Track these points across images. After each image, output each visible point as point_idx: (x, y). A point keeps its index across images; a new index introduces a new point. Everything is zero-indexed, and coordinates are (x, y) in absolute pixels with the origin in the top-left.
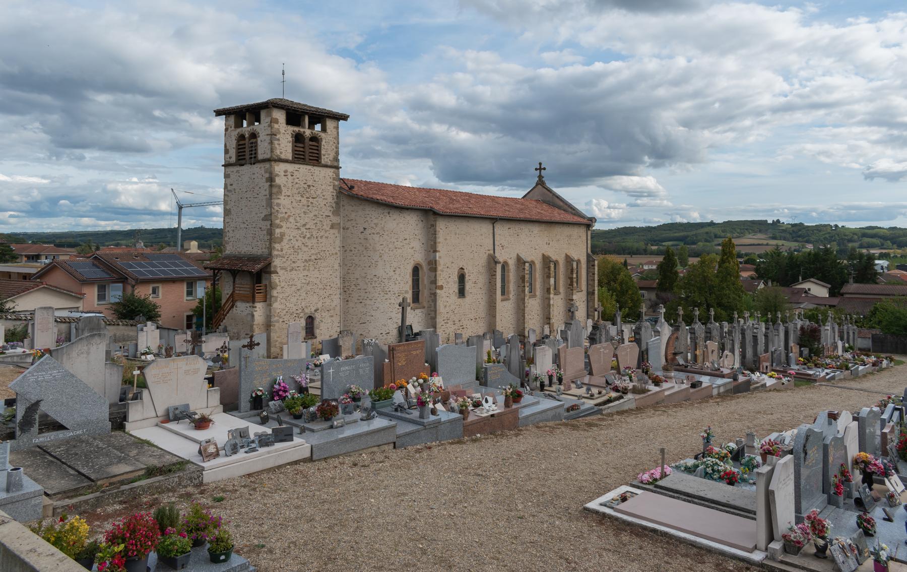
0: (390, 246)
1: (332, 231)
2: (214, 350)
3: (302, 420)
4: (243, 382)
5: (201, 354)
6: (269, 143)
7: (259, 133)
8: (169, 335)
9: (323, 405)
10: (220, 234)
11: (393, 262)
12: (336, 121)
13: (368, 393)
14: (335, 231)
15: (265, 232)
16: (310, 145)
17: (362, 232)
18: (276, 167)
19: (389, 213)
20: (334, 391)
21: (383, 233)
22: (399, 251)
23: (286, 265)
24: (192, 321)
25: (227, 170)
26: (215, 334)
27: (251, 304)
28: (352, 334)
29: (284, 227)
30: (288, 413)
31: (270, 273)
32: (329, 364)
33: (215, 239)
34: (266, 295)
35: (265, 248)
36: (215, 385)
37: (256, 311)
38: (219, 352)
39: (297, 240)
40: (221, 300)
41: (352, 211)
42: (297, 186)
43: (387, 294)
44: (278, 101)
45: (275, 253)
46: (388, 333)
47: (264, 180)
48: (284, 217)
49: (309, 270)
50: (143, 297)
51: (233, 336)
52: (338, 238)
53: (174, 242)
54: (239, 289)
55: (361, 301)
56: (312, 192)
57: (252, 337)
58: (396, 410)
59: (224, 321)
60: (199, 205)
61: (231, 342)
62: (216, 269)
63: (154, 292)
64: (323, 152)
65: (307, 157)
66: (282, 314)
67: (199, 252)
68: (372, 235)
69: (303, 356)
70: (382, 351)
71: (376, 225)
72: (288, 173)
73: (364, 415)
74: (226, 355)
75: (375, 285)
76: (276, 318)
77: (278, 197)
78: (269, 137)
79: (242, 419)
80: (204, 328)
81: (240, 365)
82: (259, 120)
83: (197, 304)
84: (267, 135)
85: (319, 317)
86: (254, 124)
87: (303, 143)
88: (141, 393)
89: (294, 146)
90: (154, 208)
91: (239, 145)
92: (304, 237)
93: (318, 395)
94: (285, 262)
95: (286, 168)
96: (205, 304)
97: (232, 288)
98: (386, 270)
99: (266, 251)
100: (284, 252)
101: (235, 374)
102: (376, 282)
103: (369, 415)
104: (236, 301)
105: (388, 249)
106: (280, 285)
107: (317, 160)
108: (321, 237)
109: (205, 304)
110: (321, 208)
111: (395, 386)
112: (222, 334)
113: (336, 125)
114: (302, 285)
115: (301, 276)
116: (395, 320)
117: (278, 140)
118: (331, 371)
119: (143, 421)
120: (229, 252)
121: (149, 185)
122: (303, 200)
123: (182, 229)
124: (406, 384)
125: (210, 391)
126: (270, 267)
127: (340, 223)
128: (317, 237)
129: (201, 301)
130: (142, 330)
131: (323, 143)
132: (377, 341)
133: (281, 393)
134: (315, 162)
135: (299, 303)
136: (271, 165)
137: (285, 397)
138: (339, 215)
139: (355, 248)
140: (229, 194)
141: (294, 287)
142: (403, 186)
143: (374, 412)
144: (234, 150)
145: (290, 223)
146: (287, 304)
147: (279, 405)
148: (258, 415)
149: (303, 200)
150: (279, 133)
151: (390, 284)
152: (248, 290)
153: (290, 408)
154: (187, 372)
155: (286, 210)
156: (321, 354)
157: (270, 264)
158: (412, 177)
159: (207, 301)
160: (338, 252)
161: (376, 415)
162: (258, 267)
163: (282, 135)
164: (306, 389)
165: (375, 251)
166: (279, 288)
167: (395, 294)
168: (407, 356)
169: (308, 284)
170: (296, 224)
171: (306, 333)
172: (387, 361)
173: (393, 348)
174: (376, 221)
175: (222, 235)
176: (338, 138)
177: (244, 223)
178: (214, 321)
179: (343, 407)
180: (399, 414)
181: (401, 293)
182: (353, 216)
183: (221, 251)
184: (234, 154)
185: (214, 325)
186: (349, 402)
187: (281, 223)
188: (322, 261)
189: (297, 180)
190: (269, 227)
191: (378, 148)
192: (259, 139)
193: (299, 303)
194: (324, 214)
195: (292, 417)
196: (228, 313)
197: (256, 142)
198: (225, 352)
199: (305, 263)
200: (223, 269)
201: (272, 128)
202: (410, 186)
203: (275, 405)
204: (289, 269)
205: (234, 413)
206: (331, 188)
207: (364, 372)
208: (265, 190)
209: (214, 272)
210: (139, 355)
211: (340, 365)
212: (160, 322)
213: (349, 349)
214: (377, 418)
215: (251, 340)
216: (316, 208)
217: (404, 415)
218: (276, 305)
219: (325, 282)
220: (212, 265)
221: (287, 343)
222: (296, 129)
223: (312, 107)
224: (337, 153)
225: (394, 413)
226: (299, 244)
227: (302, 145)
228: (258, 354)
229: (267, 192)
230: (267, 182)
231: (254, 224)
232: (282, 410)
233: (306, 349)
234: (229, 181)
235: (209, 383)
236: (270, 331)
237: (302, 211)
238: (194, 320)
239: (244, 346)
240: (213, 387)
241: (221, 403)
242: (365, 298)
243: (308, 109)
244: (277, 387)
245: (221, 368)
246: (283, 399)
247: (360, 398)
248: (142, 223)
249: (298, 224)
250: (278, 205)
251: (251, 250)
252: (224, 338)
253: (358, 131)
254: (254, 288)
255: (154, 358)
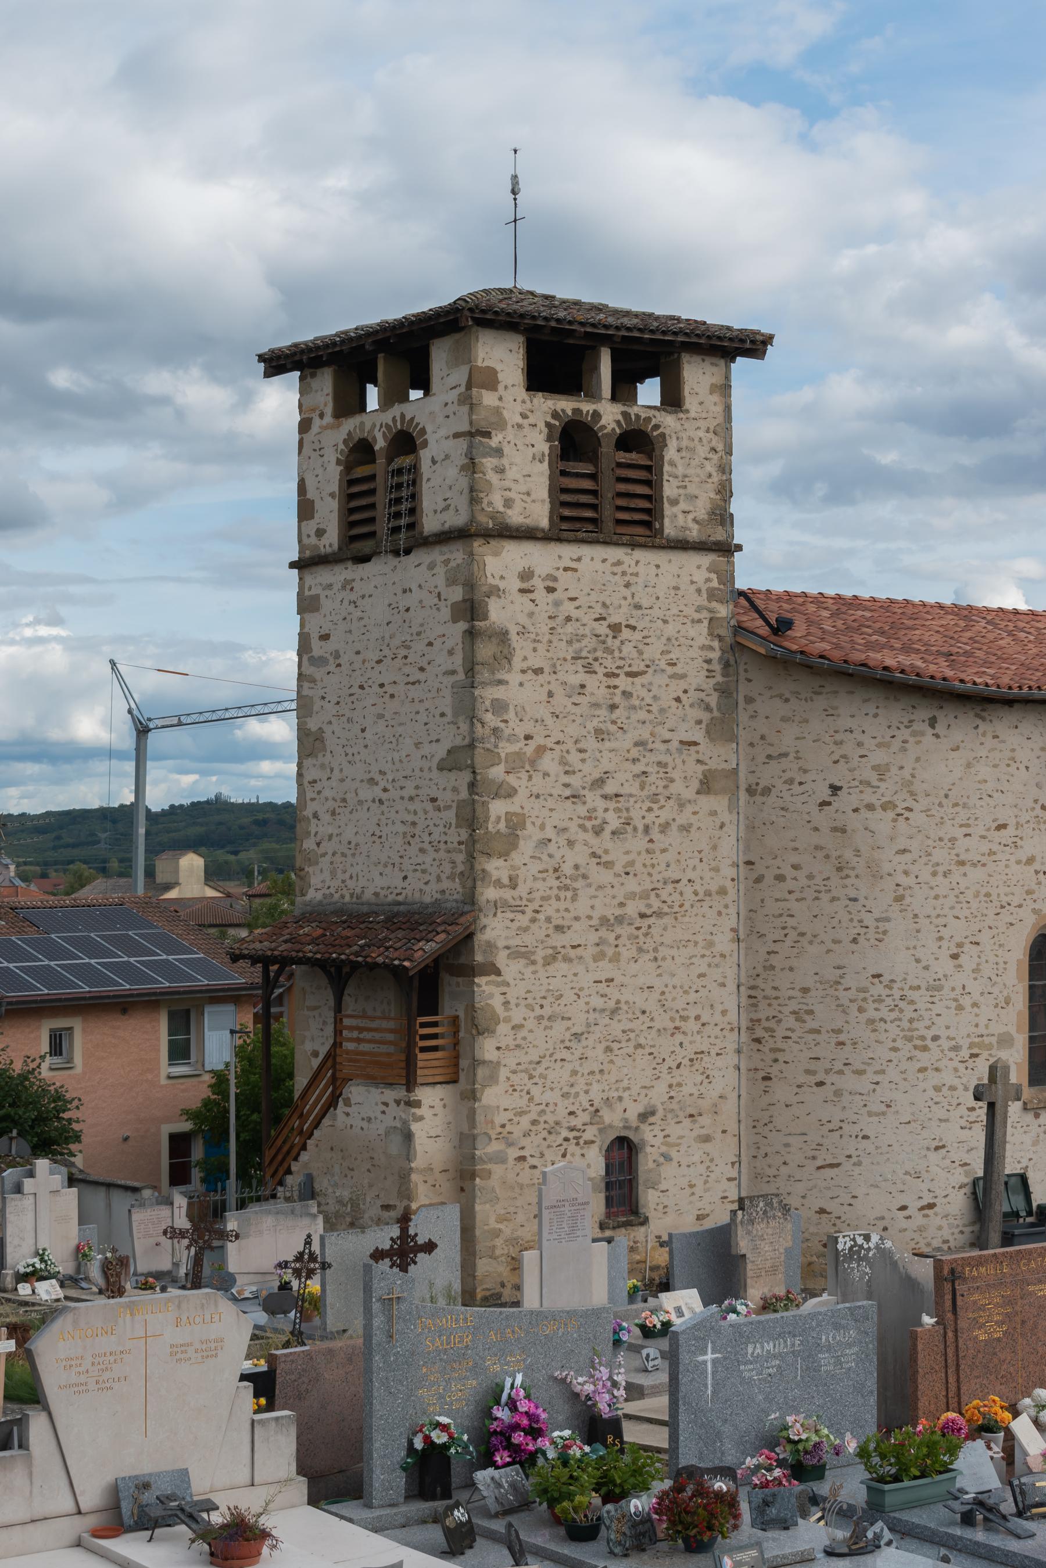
0: (940, 855)
1: (707, 803)
2: (269, 1264)
3: (599, 1546)
4: (378, 1392)
5: (225, 1282)
6: (463, 468)
7: (423, 431)
8: (109, 1206)
9: (678, 1489)
10: (281, 823)
11: (950, 920)
12: (722, 362)
13: (852, 1446)
14: (718, 803)
15: (450, 815)
16: (619, 465)
17: (824, 804)
18: (489, 560)
19: (933, 722)
20: (719, 1435)
21: (910, 803)
22: (976, 874)
23: (528, 939)
24: (188, 1154)
25: (309, 580)
26: (270, 1206)
27: (401, 1093)
28: (786, 1209)
29: (523, 793)
30: (547, 1515)
31: (469, 971)
32: (701, 1330)
33: (266, 845)
34: (457, 1057)
35: (451, 877)
36: (278, 1401)
37: (421, 1118)
38: (288, 1275)
39: (571, 843)
40: (291, 1076)
41: (784, 719)
42: (570, 628)
43: (925, 1049)
44: (495, 298)
45: (488, 893)
46: (931, 1206)
47: (446, 613)
48: (519, 754)
49: (616, 959)
50: (18, 1067)
51: (337, 1215)
52: (731, 829)
53: (121, 861)
54: (355, 1034)
55: (819, 1078)
56: (628, 649)
57: (405, 1220)
58: (968, 1519)
59: (304, 1157)
60: (208, 716)
61: (332, 1238)
62: (273, 960)
63: (57, 1046)
64: (669, 490)
65: (608, 513)
66: (517, 1131)
67: (210, 893)
68: (864, 813)
69: (599, 1296)
70: (910, 1283)
71: (881, 771)
72: (537, 583)
73: (841, 1534)
74: (314, 1286)
75: (877, 1015)
76: (495, 1147)
77: (499, 676)
78: (462, 444)
79: (376, 1530)
80: (232, 1182)
81: (368, 1327)
82: (423, 383)
83: (206, 1093)
84: (456, 436)
85: (657, 1142)
86: (405, 398)
87: (593, 457)
88: (22, 1422)
89: (558, 474)
90: (55, 734)
91: (351, 483)
92: (598, 831)
93: (659, 1450)
94: (526, 929)
95: (521, 565)
96: (233, 1090)
97: (330, 1030)
98: (920, 953)
99: (454, 889)
100: (522, 890)
101: (350, 1360)
102: (879, 1000)
103: (858, 1535)
104: (347, 1080)
105: (929, 869)
106: (508, 1020)
107: (648, 524)
108: (665, 828)
109: (233, 1090)
110: (662, 711)
111: (961, 1422)
112: (297, 1205)
113: (718, 379)
114: (592, 1016)
115: (586, 980)
116: (959, 1155)
117: (499, 452)
118: (709, 1357)
119: (31, 1527)
120: (319, 896)
121: (37, 649)
122: (591, 682)
123: (148, 811)
124: (1007, 1415)
125: (261, 1422)
126: (472, 951)
127: (735, 771)
128: (647, 829)
129: (220, 1080)
130: (18, 1189)
131: (670, 453)
132: (888, 1244)
133: (518, 1438)
134: (640, 530)
135: (580, 1087)
136: (471, 554)
137: (533, 1456)
138: (733, 738)
139: (796, 867)
140: (318, 673)
141: (559, 1027)
142: (989, 610)
143: (879, 1526)
144: (334, 505)
145: (546, 774)
146: (536, 1091)
147: (513, 1485)
148: (436, 1519)
149: (591, 682)
150: (502, 424)
151: (937, 1008)
152: (390, 1037)
153: (552, 1496)
154: (178, 1352)
155: (528, 727)
156: (666, 1286)
157: (470, 936)
158: (1029, 567)
159: (243, 1078)
160: (729, 884)
161: (887, 1535)
162: (428, 948)
163: (510, 433)
164: (614, 1426)
165: (877, 876)
166: (503, 1029)
167: (956, 1048)
168: (1009, 1302)
169: (615, 1011)
170: (566, 779)
171: (609, 1202)
172: (928, 1320)
173: (952, 1271)
174: (879, 757)
175: (293, 827)
176: (729, 429)
177: (372, 781)
178: (268, 1155)
179: (758, 1500)
180: (979, 1535)
181: (978, 1045)
182: (787, 740)
183: (288, 890)
184: (335, 515)
185: (270, 1171)
186: (778, 1482)
187: (511, 779)
188: (667, 920)
189: (568, 608)
190: (464, 794)
191: (888, 458)
192: (425, 455)
193: (580, 1087)
194: (676, 738)
195: (562, 1531)
196: (317, 1124)
197: (415, 468)
198: (310, 1274)
199: (603, 933)
200: (299, 962)
201: (472, 407)
202: (1023, 607)
203: (499, 1485)
204: (540, 955)
205: (348, 1508)
206: (700, 634)
207: (838, 1363)
208: (451, 653)
209: (266, 972)
210: (9, 1282)
211: (741, 1336)
212: (78, 1161)
213: (774, 1269)
214: (892, 1550)
215: (404, 1230)
216: (642, 715)
217: (998, 1541)
218: (492, 1096)
219: (680, 1004)
220: (258, 945)
221: (537, 1244)
222: (566, 405)
223: (627, 313)
224: (725, 491)
225: (958, 1531)
226: (579, 856)
227: (586, 468)
228: (431, 1285)
229: (458, 660)
230: (455, 620)
231: (410, 785)
232: (523, 1505)
233: (611, 1267)
234: (315, 622)
235: (257, 1395)
236: (474, 1198)
237: (591, 725)
238: (198, 1152)
239: (378, 1255)
240: (270, 1407)
241: (301, 1471)
242: (838, 1066)
243: (611, 320)
244: (502, 1414)
245: (298, 1336)
246: (526, 1460)
247: (823, 1468)
248: (13, 791)
249: (575, 781)
250: (499, 707)
251: (400, 884)
252: (306, 1221)
253: (807, 394)
254: (410, 1032)
255: (59, 1293)
